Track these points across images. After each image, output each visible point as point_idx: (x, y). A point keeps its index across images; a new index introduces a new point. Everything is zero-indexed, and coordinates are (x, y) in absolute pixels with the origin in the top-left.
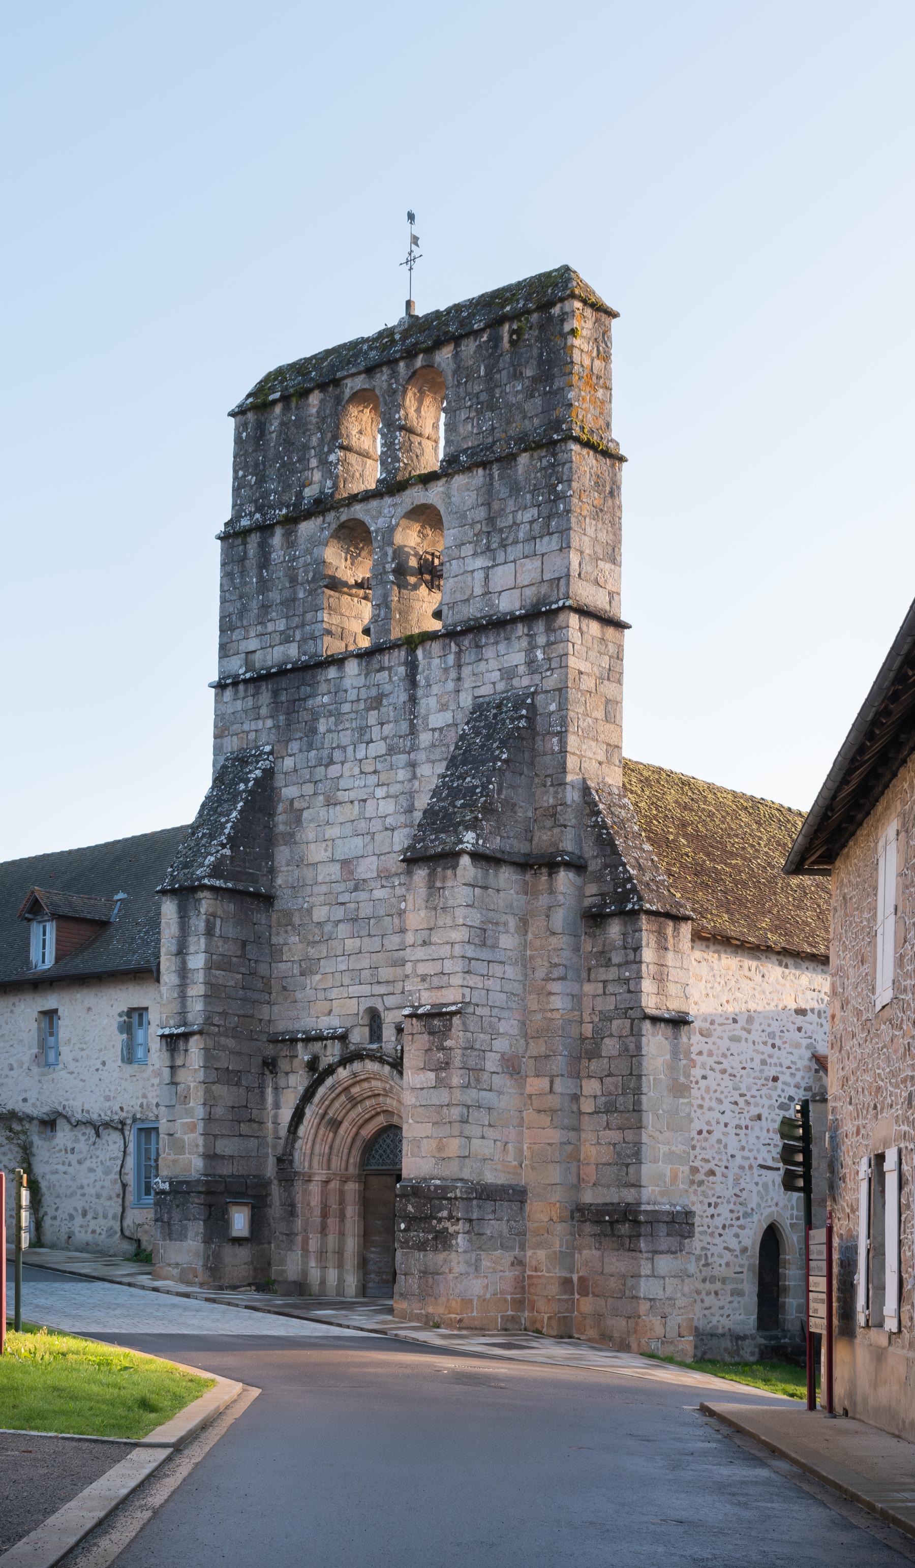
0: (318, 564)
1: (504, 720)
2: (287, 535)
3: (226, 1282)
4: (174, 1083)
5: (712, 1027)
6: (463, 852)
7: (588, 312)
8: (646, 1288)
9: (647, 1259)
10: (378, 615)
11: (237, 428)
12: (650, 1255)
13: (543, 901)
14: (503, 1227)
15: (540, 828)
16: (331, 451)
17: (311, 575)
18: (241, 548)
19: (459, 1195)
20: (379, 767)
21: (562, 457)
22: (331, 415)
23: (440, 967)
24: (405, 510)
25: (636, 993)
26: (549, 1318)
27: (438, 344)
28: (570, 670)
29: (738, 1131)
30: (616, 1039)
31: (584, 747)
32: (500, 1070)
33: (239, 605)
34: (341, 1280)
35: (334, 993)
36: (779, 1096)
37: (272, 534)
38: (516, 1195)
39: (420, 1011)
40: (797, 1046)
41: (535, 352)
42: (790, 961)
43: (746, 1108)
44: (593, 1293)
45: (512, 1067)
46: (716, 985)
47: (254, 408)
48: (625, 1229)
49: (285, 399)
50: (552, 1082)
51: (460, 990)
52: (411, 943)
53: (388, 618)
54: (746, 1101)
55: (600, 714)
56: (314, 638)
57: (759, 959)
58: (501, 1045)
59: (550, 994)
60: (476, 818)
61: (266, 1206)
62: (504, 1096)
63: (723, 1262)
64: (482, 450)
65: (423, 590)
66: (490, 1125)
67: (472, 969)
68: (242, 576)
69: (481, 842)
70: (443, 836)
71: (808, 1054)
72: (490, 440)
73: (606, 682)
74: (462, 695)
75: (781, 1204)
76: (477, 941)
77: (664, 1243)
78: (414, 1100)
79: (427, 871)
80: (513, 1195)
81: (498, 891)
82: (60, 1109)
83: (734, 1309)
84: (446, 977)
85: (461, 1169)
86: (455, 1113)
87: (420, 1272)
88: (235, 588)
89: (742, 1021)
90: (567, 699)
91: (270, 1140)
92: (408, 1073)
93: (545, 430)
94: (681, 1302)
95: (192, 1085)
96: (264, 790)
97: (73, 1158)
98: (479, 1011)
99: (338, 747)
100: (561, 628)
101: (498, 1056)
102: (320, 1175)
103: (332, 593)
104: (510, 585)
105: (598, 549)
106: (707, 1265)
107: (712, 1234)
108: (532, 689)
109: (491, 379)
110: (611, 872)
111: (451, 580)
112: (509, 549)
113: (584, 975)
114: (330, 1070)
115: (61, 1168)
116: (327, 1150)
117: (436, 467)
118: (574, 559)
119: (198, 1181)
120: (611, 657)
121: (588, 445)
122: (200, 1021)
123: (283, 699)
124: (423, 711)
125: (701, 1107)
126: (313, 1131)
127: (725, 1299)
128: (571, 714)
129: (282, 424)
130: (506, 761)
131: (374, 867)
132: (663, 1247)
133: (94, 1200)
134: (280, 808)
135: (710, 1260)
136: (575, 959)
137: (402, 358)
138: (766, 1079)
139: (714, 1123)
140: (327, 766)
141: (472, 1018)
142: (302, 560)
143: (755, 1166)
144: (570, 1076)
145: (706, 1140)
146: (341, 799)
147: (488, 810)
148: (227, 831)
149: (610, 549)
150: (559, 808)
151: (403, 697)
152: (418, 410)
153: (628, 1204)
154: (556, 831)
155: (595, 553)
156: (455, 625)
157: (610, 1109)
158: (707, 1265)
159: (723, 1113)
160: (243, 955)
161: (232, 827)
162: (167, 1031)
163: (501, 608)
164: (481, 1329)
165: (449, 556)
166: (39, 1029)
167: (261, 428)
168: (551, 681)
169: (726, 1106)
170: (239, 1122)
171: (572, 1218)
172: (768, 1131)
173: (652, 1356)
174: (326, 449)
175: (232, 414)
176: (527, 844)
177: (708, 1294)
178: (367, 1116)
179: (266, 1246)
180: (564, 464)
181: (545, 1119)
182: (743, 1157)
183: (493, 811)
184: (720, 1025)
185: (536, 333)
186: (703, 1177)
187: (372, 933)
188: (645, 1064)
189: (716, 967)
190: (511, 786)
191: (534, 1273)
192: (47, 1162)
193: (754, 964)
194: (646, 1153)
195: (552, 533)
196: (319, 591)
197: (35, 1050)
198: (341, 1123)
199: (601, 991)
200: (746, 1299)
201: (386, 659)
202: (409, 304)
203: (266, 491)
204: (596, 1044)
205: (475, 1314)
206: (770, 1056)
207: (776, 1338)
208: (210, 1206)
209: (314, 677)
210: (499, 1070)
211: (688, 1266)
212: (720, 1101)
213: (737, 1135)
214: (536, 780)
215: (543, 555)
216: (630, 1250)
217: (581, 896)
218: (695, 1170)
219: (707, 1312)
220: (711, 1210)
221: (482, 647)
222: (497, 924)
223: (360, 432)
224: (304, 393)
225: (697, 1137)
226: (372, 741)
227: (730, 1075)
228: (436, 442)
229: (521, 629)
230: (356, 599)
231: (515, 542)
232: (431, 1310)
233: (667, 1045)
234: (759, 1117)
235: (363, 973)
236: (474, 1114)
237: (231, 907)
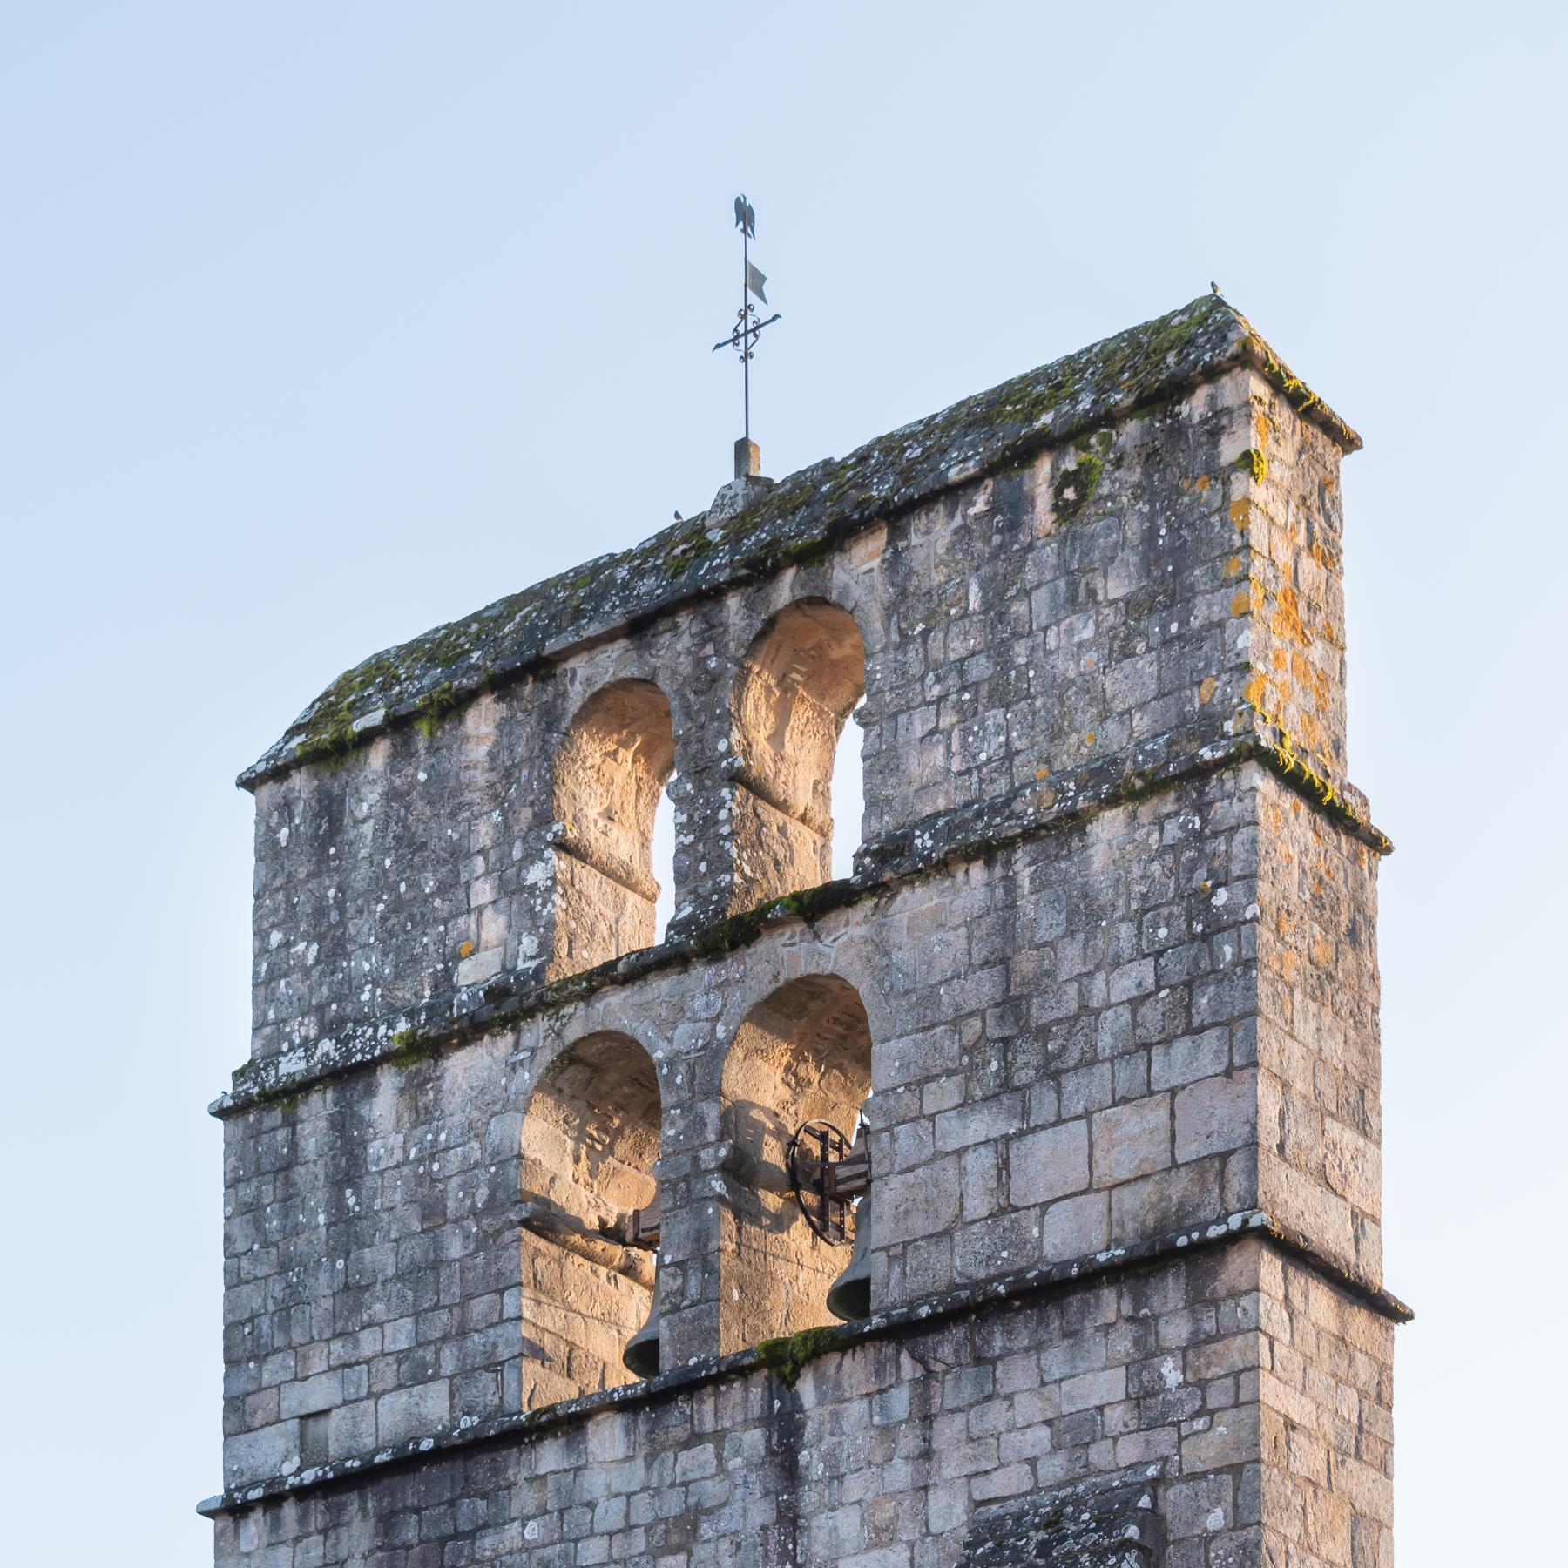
0: (502, 1164)
2: (413, 1089)
10: (682, 1292)
11: (262, 818)
16: (532, 856)
17: (482, 1194)
18: (281, 1135)
21: (1225, 812)
22: (530, 760)
24: (754, 998)
27: (842, 534)
28: (1264, 1413)
33: (277, 1289)
37: (370, 1092)
41: (1134, 528)
47: (314, 758)
49: (398, 725)
53: (710, 1299)
64: (979, 815)
65: (799, 1234)
68: (286, 1212)
72: (1002, 786)
73: (1351, 1463)
74: (938, 1501)
88: (266, 1244)
90: (1257, 1494)
93: (1170, 744)
100: (1235, 1294)
103: (542, 1244)
104: (1077, 1184)
105: (1325, 1083)
108: (1152, 1471)
109: (1001, 616)
111: (895, 1182)
112: (1070, 1083)
117: (842, 869)
120: (1362, 1394)
121: (1294, 781)
123: (411, 1535)
128: (1270, 1539)
129: (392, 795)
137: (735, 584)
142: (454, 1157)
149: (1353, 1090)
151: (761, 1513)
152: (776, 738)
155: (1318, 1095)
156: (912, 1305)
163: (1048, 1250)
165: (887, 1113)
167: (330, 810)
168: (1210, 1445)
174: (517, 853)
175: (250, 782)
180: (1234, 829)
185: (1136, 475)
195: (1202, 1029)
196: (508, 1236)
201: (706, 1412)
202: (743, 449)
203: (349, 978)
209: (496, 1471)
221: (993, 1362)
224: (452, 707)
228: (824, 832)
229: (1110, 1303)
230: (603, 1271)
231: (1090, 1061)
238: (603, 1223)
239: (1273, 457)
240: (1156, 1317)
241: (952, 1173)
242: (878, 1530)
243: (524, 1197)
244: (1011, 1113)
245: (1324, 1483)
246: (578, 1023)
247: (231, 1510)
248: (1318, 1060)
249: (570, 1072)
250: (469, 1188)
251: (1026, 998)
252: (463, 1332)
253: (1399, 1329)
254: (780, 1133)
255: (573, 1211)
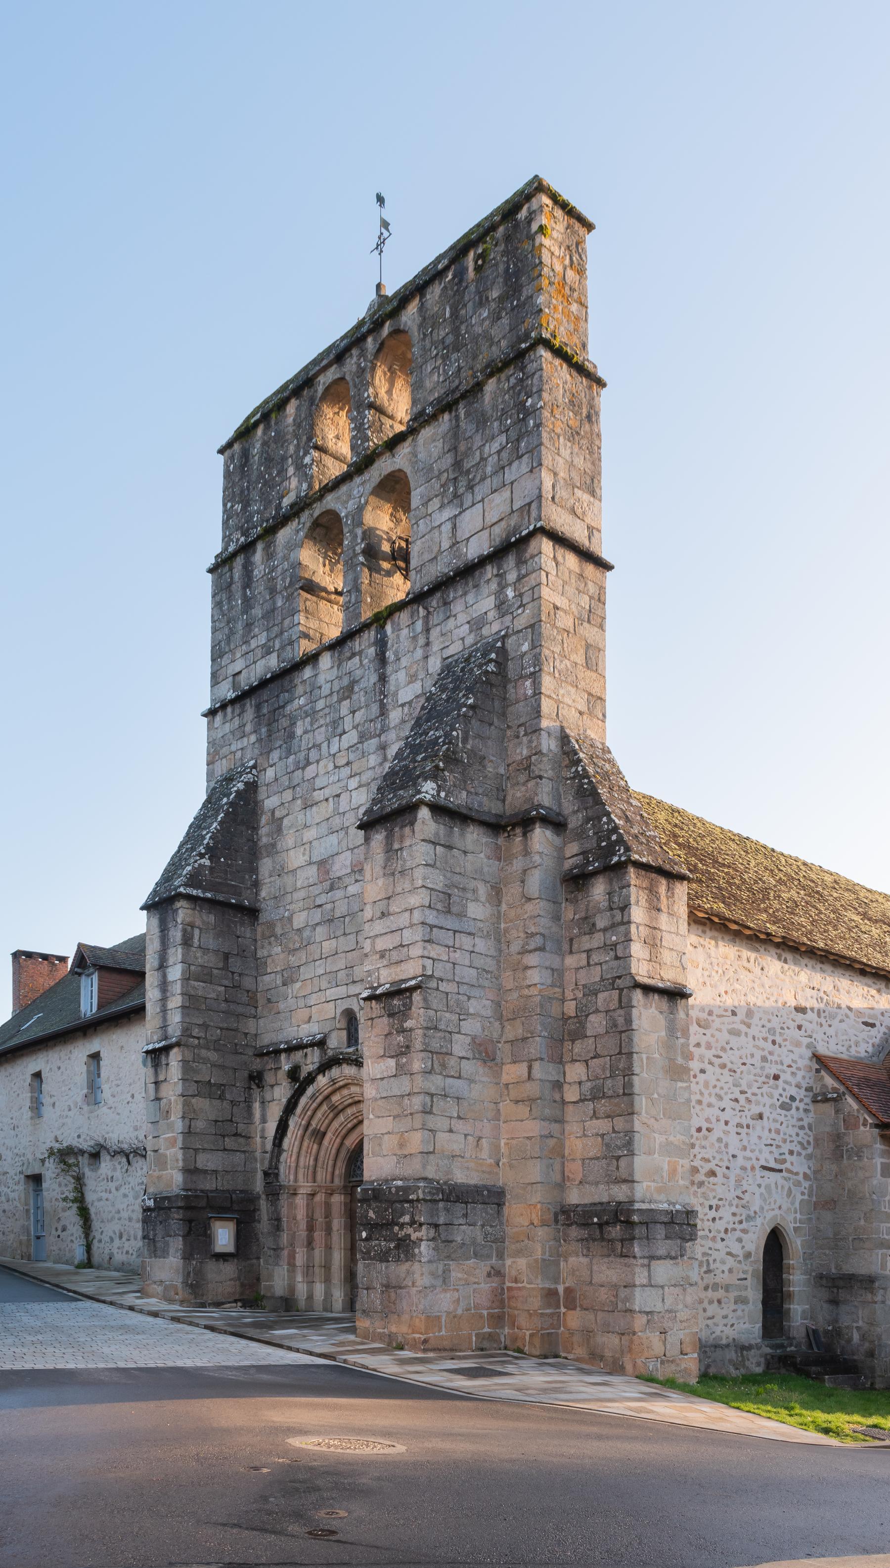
0: (294, 568)
1: (472, 669)
3: (209, 1298)
4: (158, 1099)
5: (710, 1018)
6: (422, 802)
7: (559, 213)
8: (642, 1299)
9: (643, 1266)
10: (349, 602)
12: (646, 1261)
13: (518, 864)
14: (477, 1233)
15: (513, 786)
16: (306, 453)
17: (288, 580)
19: (421, 1196)
20: (352, 757)
21: (531, 367)
23: (399, 939)
25: (624, 958)
26: (531, 1335)
29: (739, 1130)
30: (602, 1015)
31: (562, 692)
32: (470, 1055)
33: (226, 630)
34: (328, 1295)
35: (313, 1000)
36: (781, 1095)
37: (254, 552)
38: (493, 1198)
39: (378, 992)
40: (798, 1044)
41: (501, 268)
42: (789, 956)
43: (747, 1106)
44: (581, 1306)
45: (485, 1053)
46: (714, 973)
48: (616, 1231)
50: (530, 1068)
51: (420, 962)
52: (369, 917)
54: (747, 1098)
55: (580, 658)
56: (291, 643)
57: (758, 951)
58: (471, 1027)
59: (527, 968)
60: (437, 767)
61: (254, 1221)
62: (477, 1085)
63: (726, 1269)
66: (459, 1117)
67: (434, 937)
69: (443, 794)
70: (401, 792)
71: (809, 1054)
72: (457, 382)
73: (585, 624)
74: (431, 660)
75: (784, 1207)
76: (439, 906)
77: (662, 1247)
78: (374, 1092)
79: (384, 834)
80: (489, 1196)
81: (465, 852)
82: (102, 1142)
83: (738, 1318)
84: (406, 949)
85: (424, 1166)
86: (417, 1102)
87: (383, 1285)
89: (741, 1015)
91: (258, 1154)
92: (368, 1063)
94: (682, 1315)
95: (173, 1099)
96: (247, 803)
97: (112, 1186)
98: (443, 986)
99: (314, 746)
101: (468, 1040)
102: (305, 1187)
103: (309, 596)
106: (708, 1271)
107: (714, 1239)
108: (503, 633)
109: (457, 317)
110: (593, 826)
111: (419, 542)
112: (476, 489)
113: (566, 947)
114: (311, 1079)
115: (104, 1195)
116: (312, 1163)
118: (547, 481)
119: (177, 1196)
120: (591, 598)
121: (559, 353)
122: (178, 1033)
123: (265, 711)
124: (392, 688)
125: (700, 1102)
126: (297, 1143)
127: (728, 1308)
128: (546, 652)
129: (265, 444)
130: (472, 707)
131: (348, 863)
132: (661, 1252)
133: (127, 1222)
134: (264, 820)
135: (712, 1267)
136: (554, 929)
138: (767, 1077)
139: (714, 1120)
140: (303, 768)
141: (435, 993)
142: (279, 569)
143: (757, 1167)
144: (552, 1060)
145: (706, 1138)
146: (317, 799)
147: (452, 759)
148: (205, 842)
150: (534, 758)
151: (374, 678)
152: (389, 392)
153: (619, 1203)
154: (531, 784)
157: (597, 1095)
158: (708, 1271)
159: (723, 1110)
160: (226, 968)
161: (211, 838)
162: (150, 1047)
164: (452, 1350)
166: (88, 1072)
167: (246, 455)
168: (523, 619)
169: (726, 1103)
170: (224, 1136)
171: (556, 1221)
172: (770, 1130)
173: (649, 1379)
176: (499, 804)
177: (711, 1302)
178: (349, 1125)
179: (255, 1261)
180: (534, 374)
181: (523, 1110)
182: (745, 1158)
183: (458, 761)
184: (719, 1016)
186: (703, 1178)
187: (347, 931)
188: (636, 1039)
189: (713, 954)
190: (478, 736)
191: (514, 1285)
192: (94, 1191)
193: (753, 955)
194: (640, 1143)
195: (523, 455)
197: (85, 1091)
198: (324, 1134)
199: (584, 963)
200: (751, 1306)
202: (379, 286)
204: (580, 1023)
205: (443, 1333)
206: (771, 1053)
207: (781, 1346)
208: (190, 1221)
209: (291, 681)
210: (470, 1055)
211: (690, 1274)
212: (720, 1098)
213: (738, 1133)
214: (509, 733)
215: (512, 483)
216: (622, 1256)
217: (561, 858)
218: (695, 1170)
219: (710, 1322)
220: (713, 1214)
221: (450, 603)
222: (464, 889)
223: (337, 437)
225: (696, 1134)
226: (345, 733)
227: (730, 1070)
229: (490, 571)
230: (336, 607)
231: (483, 479)
232: (394, 1329)
233: (661, 1020)
234: (761, 1116)
235: (340, 974)
236: (440, 1105)
237: (212, 918)
238: (336, 589)
239: (553, 229)
240: (505, 573)
241: (437, 534)
242: (411, 676)
243: (301, 578)
244: (457, 506)
245: (572, 631)
246: (318, 509)
247: (211, 713)
248: (571, 465)
249: (318, 530)
250: (283, 580)
251: (462, 460)
252: (282, 633)
253: (609, 574)
254: (389, 540)
255: (323, 584)
